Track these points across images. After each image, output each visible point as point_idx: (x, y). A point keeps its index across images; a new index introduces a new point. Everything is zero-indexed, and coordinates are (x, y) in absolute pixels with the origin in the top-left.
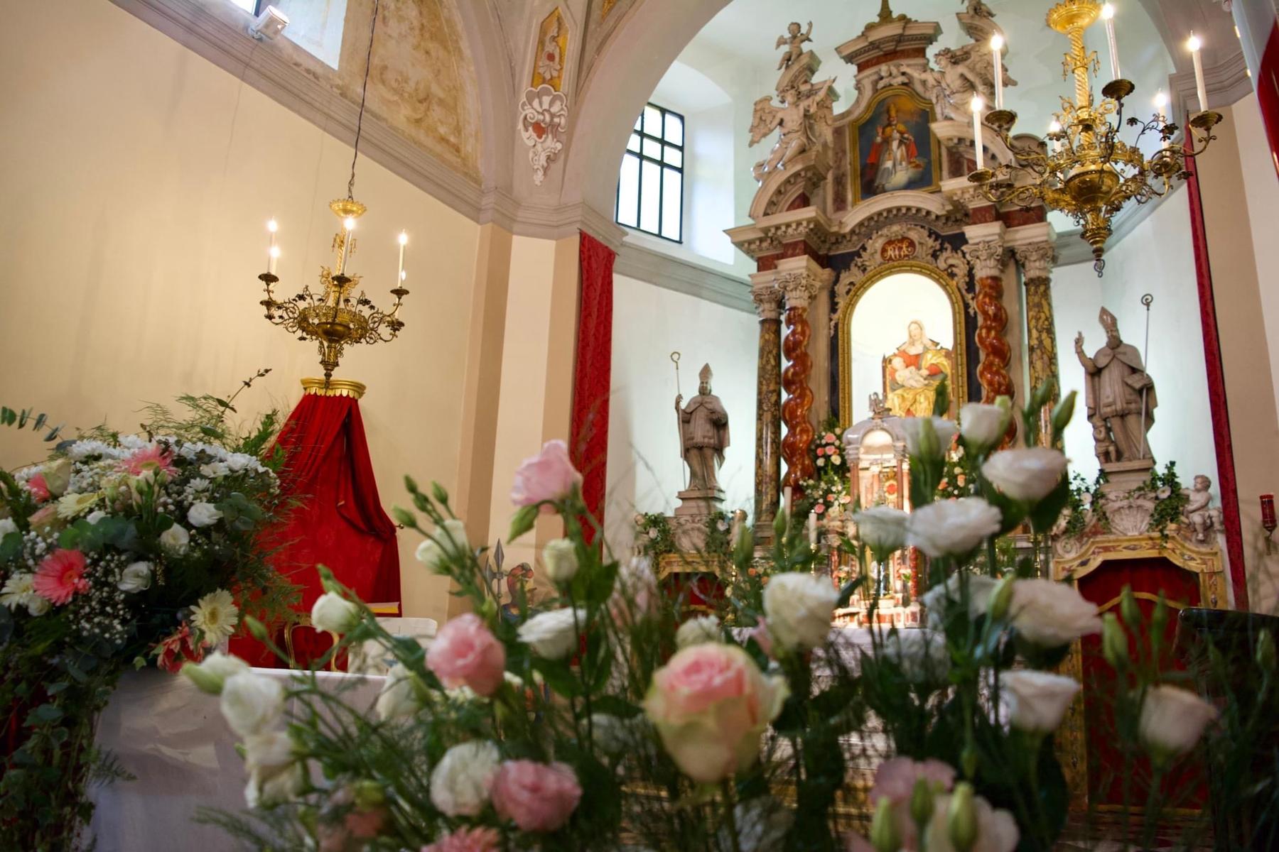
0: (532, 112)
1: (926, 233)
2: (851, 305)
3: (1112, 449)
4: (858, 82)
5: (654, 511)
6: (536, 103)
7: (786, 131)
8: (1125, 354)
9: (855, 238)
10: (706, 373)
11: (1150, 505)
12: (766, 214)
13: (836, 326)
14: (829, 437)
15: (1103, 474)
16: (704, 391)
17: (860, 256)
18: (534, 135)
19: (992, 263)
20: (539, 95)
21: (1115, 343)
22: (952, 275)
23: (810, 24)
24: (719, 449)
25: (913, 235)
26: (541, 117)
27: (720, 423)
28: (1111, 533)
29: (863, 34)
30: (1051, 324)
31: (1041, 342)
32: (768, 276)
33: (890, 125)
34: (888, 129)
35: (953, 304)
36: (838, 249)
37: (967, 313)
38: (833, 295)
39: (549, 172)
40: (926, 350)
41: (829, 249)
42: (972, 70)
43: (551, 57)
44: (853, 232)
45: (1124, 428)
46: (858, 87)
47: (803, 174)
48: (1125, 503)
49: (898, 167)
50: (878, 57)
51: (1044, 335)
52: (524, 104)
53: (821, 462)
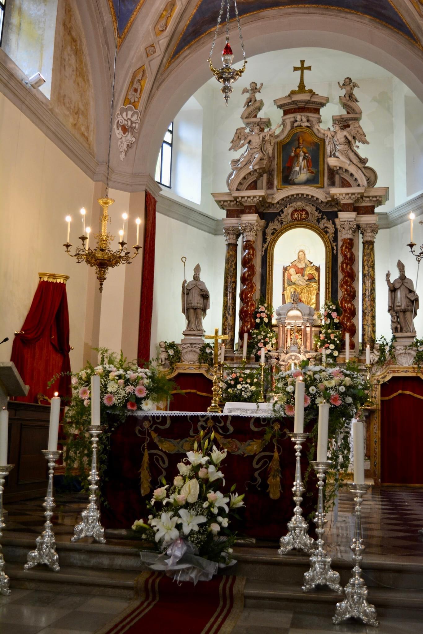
0: (121, 119)
1: (315, 209)
2: (275, 241)
3: (399, 326)
4: (284, 121)
5: (170, 341)
6: (124, 114)
7: (252, 147)
8: (407, 283)
9: (278, 206)
10: (197, 269)
11: (414, 353)
12: (237, 190)
13: (266, 250)
14: (262, 308)
15: (394, 338)
16: (196, 278)
17: (280, 216)
18: (122, 133)
19: (350, 232)
20: (126, 110)
21: (403, 277)
22: (327, 232)
23: (262, 84)
24: (204, 310)
25: (308, 209)
26: (126, 123)
27: (205, 296)
28: (396, 364)
29: (289, 96)
30: (374, 264)
31: (369, 272)
32: (233, 221)
33: (299, 147)
34: (298, 150)
35: (326, 247)
36: (268, 210)
37: (333, 252)
38: (264, 234)
39: (128, 154)
40: (307, 266)
41: (264, 210)
42: (350, 134)
43: (136, 90)
44: (278, 203)
45: (405, 318)
46: (284, 123)
47: (258, 171)
48: (403, 351)
49: (302, 172)
50: (295, 109)
51: (371, 269)
52: (118, 114)
53: (258, 321)
